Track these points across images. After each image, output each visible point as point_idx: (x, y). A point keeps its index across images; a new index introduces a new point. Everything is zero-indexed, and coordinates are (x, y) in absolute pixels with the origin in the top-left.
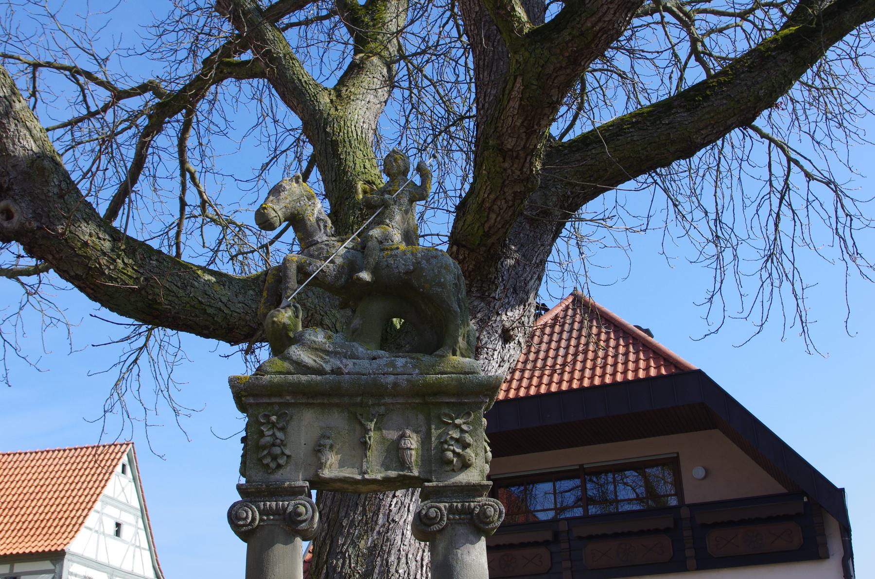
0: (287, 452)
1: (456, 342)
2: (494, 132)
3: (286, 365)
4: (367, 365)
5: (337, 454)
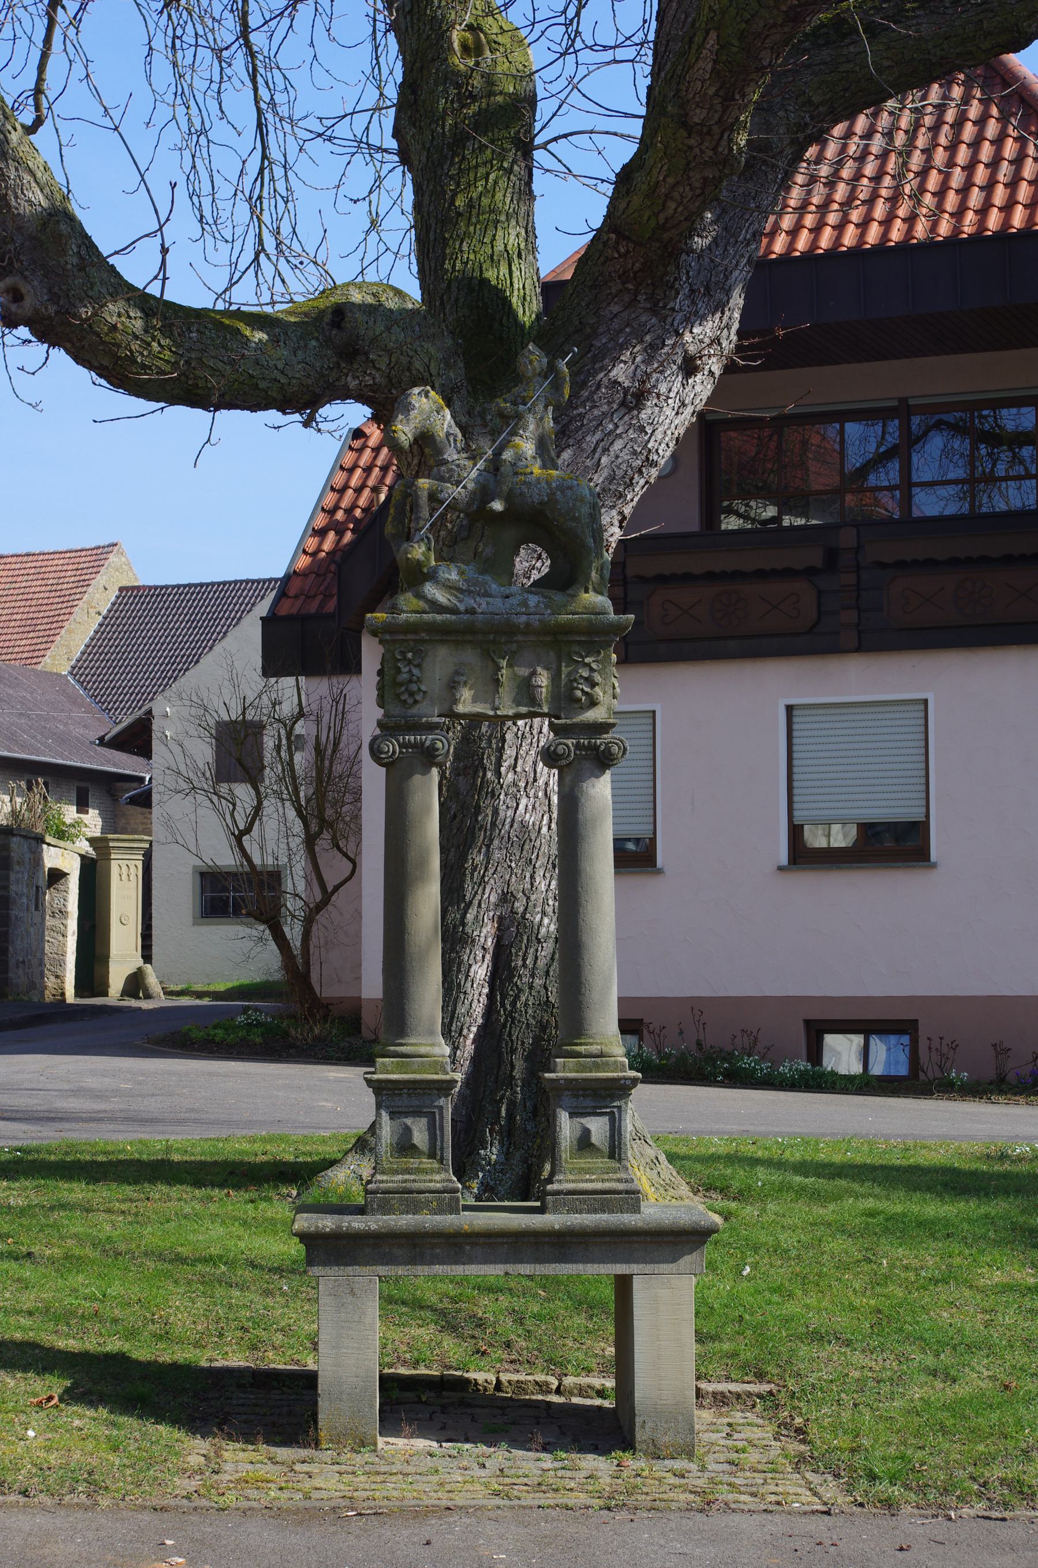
0: (423, 688)
1: (588, 577)
2: (674, 96)
3: (422, 604)
4: (500, 605)
5: (470, 689)
